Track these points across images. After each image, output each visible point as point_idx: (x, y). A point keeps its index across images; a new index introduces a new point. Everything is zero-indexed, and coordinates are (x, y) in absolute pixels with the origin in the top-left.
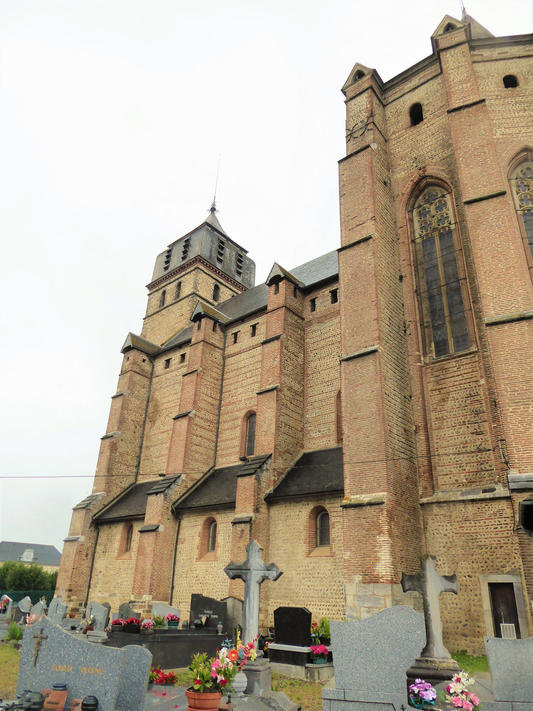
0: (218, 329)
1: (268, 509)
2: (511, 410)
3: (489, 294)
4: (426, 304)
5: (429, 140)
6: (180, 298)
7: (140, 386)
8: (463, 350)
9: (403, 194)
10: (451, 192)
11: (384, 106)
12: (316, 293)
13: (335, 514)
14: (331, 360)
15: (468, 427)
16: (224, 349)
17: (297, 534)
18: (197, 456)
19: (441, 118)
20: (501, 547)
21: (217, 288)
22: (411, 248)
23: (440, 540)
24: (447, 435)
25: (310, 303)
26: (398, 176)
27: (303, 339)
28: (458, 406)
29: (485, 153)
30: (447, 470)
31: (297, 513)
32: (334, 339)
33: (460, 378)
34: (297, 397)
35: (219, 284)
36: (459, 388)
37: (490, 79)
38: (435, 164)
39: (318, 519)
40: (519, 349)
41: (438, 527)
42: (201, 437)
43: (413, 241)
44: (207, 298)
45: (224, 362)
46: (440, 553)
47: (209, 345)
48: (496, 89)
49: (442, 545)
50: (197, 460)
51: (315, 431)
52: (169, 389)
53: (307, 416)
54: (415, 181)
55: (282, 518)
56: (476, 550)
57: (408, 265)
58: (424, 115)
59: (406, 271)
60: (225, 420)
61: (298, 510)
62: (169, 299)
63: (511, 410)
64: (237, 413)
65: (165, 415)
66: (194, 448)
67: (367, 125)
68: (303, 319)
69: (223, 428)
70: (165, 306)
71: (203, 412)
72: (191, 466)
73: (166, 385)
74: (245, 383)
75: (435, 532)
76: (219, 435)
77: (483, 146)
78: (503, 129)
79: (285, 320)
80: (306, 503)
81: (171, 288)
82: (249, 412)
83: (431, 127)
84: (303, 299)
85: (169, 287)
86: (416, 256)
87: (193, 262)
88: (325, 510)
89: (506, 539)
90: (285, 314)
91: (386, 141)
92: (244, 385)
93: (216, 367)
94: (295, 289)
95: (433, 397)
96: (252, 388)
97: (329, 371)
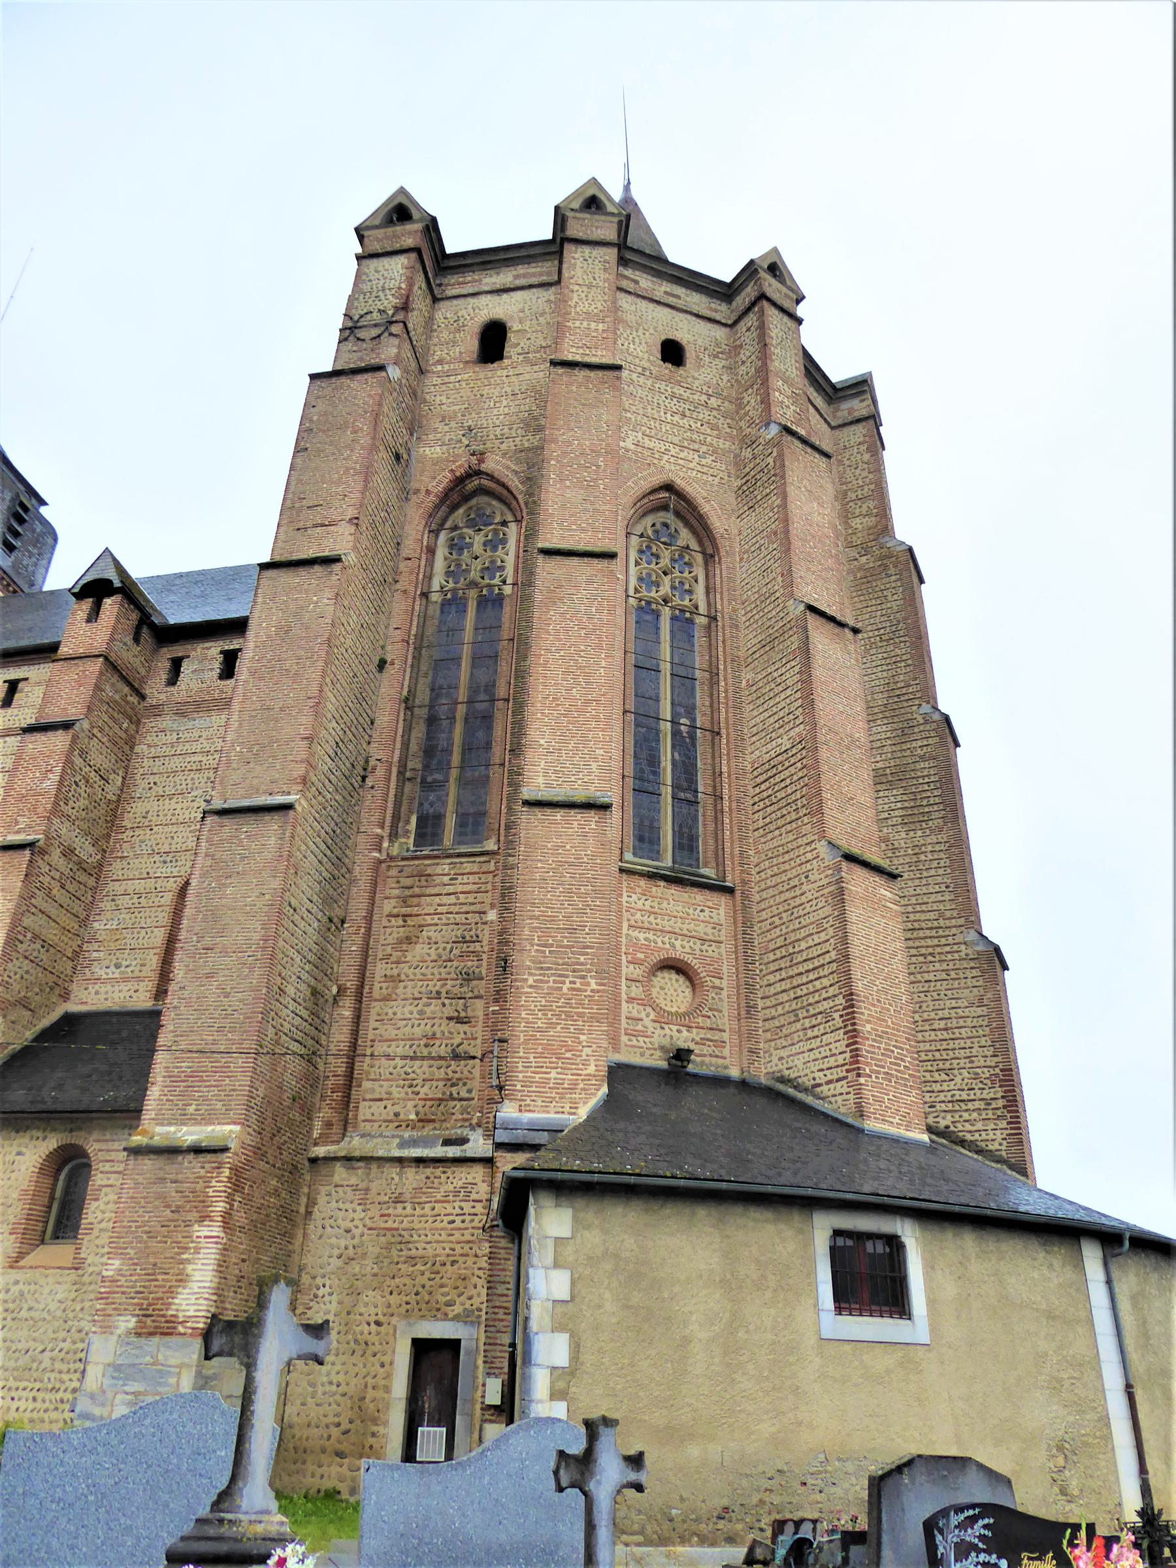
2: (531, 982)
3: (542, 742)
4: (419, 732)
9: (428, 492)
12: (189, 647)
14: (185, 805)
15: (444, 1005)
20: (453, 1263)
22: (417, 608)
24: (399, 1016)
25: (168, 665)
27: (131, 743)
28: (434, 957)
29: (598, 466)
30: (383, 1090)
32: (204, 759)
33: (452, 899)
34: (82, 877)
36: (444, 921)
43: (425, 595)
46: (329, 1269)
49: (336, 1252)
54: (458, 474)
61: (15, 1149)
63: (531, 982)
68: (143, 697)
75: (327, 1223)
80: (40, 1134)
84: (155, 651)
86: (422, 626)
95: (388, 931)
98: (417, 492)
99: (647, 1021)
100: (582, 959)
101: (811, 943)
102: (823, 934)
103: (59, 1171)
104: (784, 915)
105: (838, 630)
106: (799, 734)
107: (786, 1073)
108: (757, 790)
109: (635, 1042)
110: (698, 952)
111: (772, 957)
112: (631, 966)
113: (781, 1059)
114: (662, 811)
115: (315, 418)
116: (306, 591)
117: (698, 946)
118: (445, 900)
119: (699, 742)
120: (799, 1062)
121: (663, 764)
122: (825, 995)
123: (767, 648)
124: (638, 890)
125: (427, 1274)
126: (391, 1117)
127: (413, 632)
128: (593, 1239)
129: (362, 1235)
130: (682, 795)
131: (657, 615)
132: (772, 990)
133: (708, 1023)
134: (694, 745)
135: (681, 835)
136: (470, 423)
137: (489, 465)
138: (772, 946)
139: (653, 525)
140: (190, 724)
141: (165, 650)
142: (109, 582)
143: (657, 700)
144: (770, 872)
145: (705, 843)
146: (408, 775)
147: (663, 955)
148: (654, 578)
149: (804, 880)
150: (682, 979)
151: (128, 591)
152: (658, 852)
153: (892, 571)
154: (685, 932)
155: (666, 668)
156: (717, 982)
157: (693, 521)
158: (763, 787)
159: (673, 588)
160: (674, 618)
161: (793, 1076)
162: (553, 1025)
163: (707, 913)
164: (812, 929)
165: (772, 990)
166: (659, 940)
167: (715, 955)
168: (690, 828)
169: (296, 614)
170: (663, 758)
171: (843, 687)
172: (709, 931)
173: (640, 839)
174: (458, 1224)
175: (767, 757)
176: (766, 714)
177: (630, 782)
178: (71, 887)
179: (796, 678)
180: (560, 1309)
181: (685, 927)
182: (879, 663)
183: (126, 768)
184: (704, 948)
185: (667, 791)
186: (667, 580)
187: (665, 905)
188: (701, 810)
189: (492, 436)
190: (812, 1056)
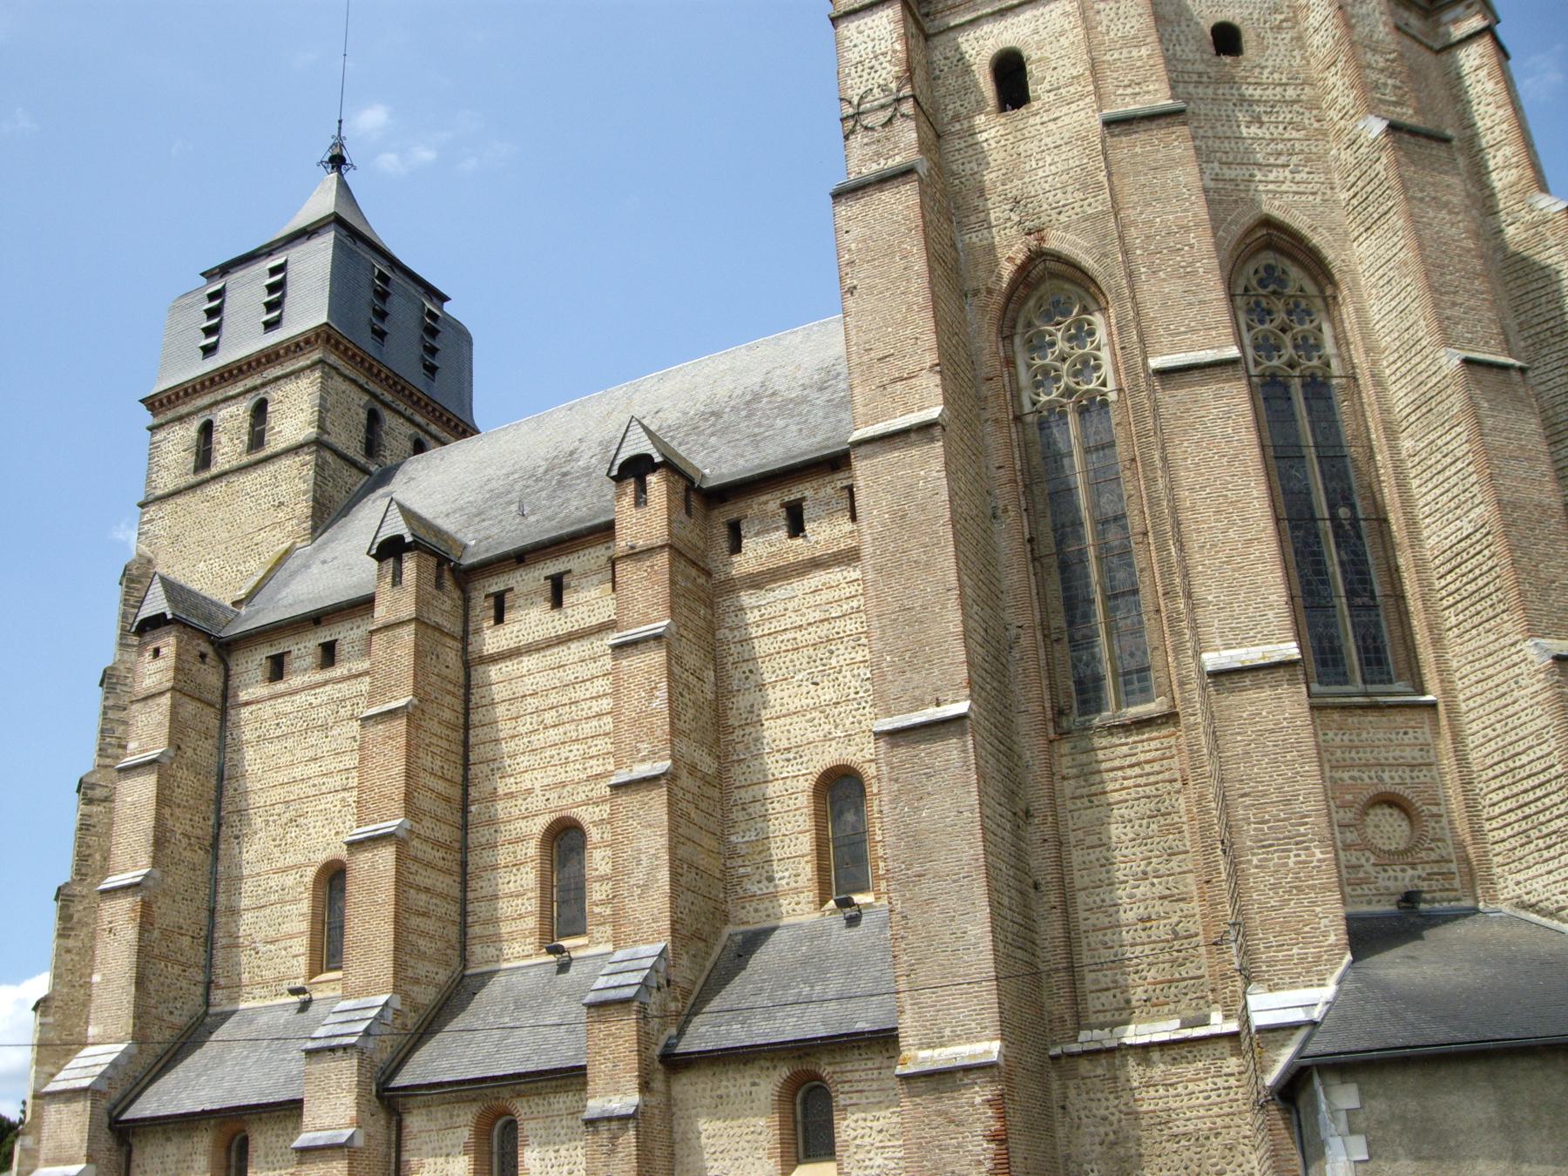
0: (448, 583)
1: (667, 1081)
2: (1255, 862)
3: (1210, 598)
4: (1055, 585)
5: (1049, 160)
6: (268, 451)
7: (199, 733)
8: (1141, 703)
9: (990, 292)
10: (1106, 309)
11: (927, 37)
12: (742, 504)
13: (847, 1087)
14: (792, 691)
15: (1153, 884)
16: (464, 639)
17: (749, 1137)
18: (422, 943)
19: (1074, 107)
20: (1217, 1135)
21: (373, 418)
22: (1014, 436)
23: (1092, 1129)
24: (1108, 902)
25: (724, 530)
26: (974, 239)
27: (712, 629)
28: (1131, 836)
29: (1191, 246)
30: (1108, 980)
31: (748, 1088)
32: (798, 635)
33: (1137, 770)
34: (709, 791)
35: (378, 406)
36: (1134, 795)
37: (1184, 27)
38: (1066, 228)
39: (798, 1100)
40: (1272, 731)
41: (1089, 1104)
42: (427, 890)
43: (1018, 419)
44: (350, 453)
45: (468, 677)
46: (1094, 1155)
47: (430, 631)
48: (1198, 56)
49: (1097, 1139)
50: (422, 956)
51: (757, 877)
52: (290, 743)
53: (733, 838)
54: (1018, 262)
55: (707, 1101)
56: (1168, 1145)
57: (1010, 481)
58: (1031, 88)
59: (1005, 495)
60: (483, 840)
61: (748, 1081)
62: (228, 450)
63: (1255, 862)
64: (522, 824)
65: (284, 820)
66: (415, 921)
67: (898, 100)
68: (708, 574)
69: (481, 863)
70: (214, 470)
71: (428, 822)
72: (410, 973)
73: (279, 732)
74: (539, 739)
75: (1083, 1114)
76: (472, 884)
77: (1187, 229)
78: (1216, 164)
79: (672, 582)
80: (768, 1064)
81: (232, 418)
82: (559, 821)
83: (1051, 126)
84: (706, 517)
85: (222, 416)
86: (1026, 459)
87: (307, 342)
88: (820, 1079)
89: (1227, 1119)
90: (671, 565)
91: (939, 136)
92: (536, 745)
93: (449, 692)
94: (687, 490)
95: (1076, 814)
96: (563, 756)
97: (788, 721)
98: (976, 293)
99: (1368, 867)
100: (1302, 829)
101: (1532, 756)
102: (1544, 746)
103: (795, 1095)
104: (1498, 726)
105: (1502, 377)
106: (1480, 516)
107: (1526, 898)
108: (1443, 582)
109: (1359, 892)
110: (1408, 781)
111: (1491, 773)
112: (1341, 811)
113: (1518, 883)
114: (1341, 628)
115: (853, 246)
116: (910, 465)
117: (1407, 775)
118: (1129, 772)
119: (1364, 534)
120: (1537, 885)
121: (1330, 570)
122: (1556, 812)
123: (1424, 410)
124: (1334, 725)
125: (1193, 1149)
126: (1123, 1005)
127: (1018, 467)
128: (1380, 1106)
129: (1120, 1121)
130: (1359, 601)
131: (1286, 387)
132: (1497, 810)
133: (1434, 856)
134: (1360, 537)
135: (1367, 650)
136: (1015, 192)
137: (1053, 243)
138: (1489, 761)
139: (1256, 272)
140: (770, 596)
141: (716, 512)
142: (648, 457)
143: (1309, 494)
144: (1473, 678)
145: (1394, 653)
146: (1054, 637)
147: (1372, 791)
148: (1272, 341)
149: (1514, 686)
150: (1396, 812)
151: (672, 467)
152: (1345, 674)
153: (1551, 241)
154: (1391, 761)
155: (1311, 453)
156: (1435, 809)
157: (1301, 256)
158: (1449, 578)
159: (1296, 347)
160: (1304, 386)
161: (1533, 900)
162: (1285, 902)
163: (1411, 735)
164: (1531, 741)
165: (1497, 810)
166: (1365, 776)
167: (1428, 779)
168: (1375, 639)
169: (907, 495)
170: (1328, 563)
171: (1522, 448)
172: (1417, 754)
173: (1323, 663)
174: (1214, 1098)
175: (1447, 543)
176: (1437, 491)
177: (1299, 601)
178: (703, 805)
179: (1466, 447)
180: (1360, 1167)
181: (1391, 755)
182: (1555, 365)
183: (714, 659)
184: (1415, 774)
185: (1342, 603)
186: (1287, 339)
187: (1364, 735)
188: (1382, 614)
189: (1045, 206)
190: (1551, 878)
